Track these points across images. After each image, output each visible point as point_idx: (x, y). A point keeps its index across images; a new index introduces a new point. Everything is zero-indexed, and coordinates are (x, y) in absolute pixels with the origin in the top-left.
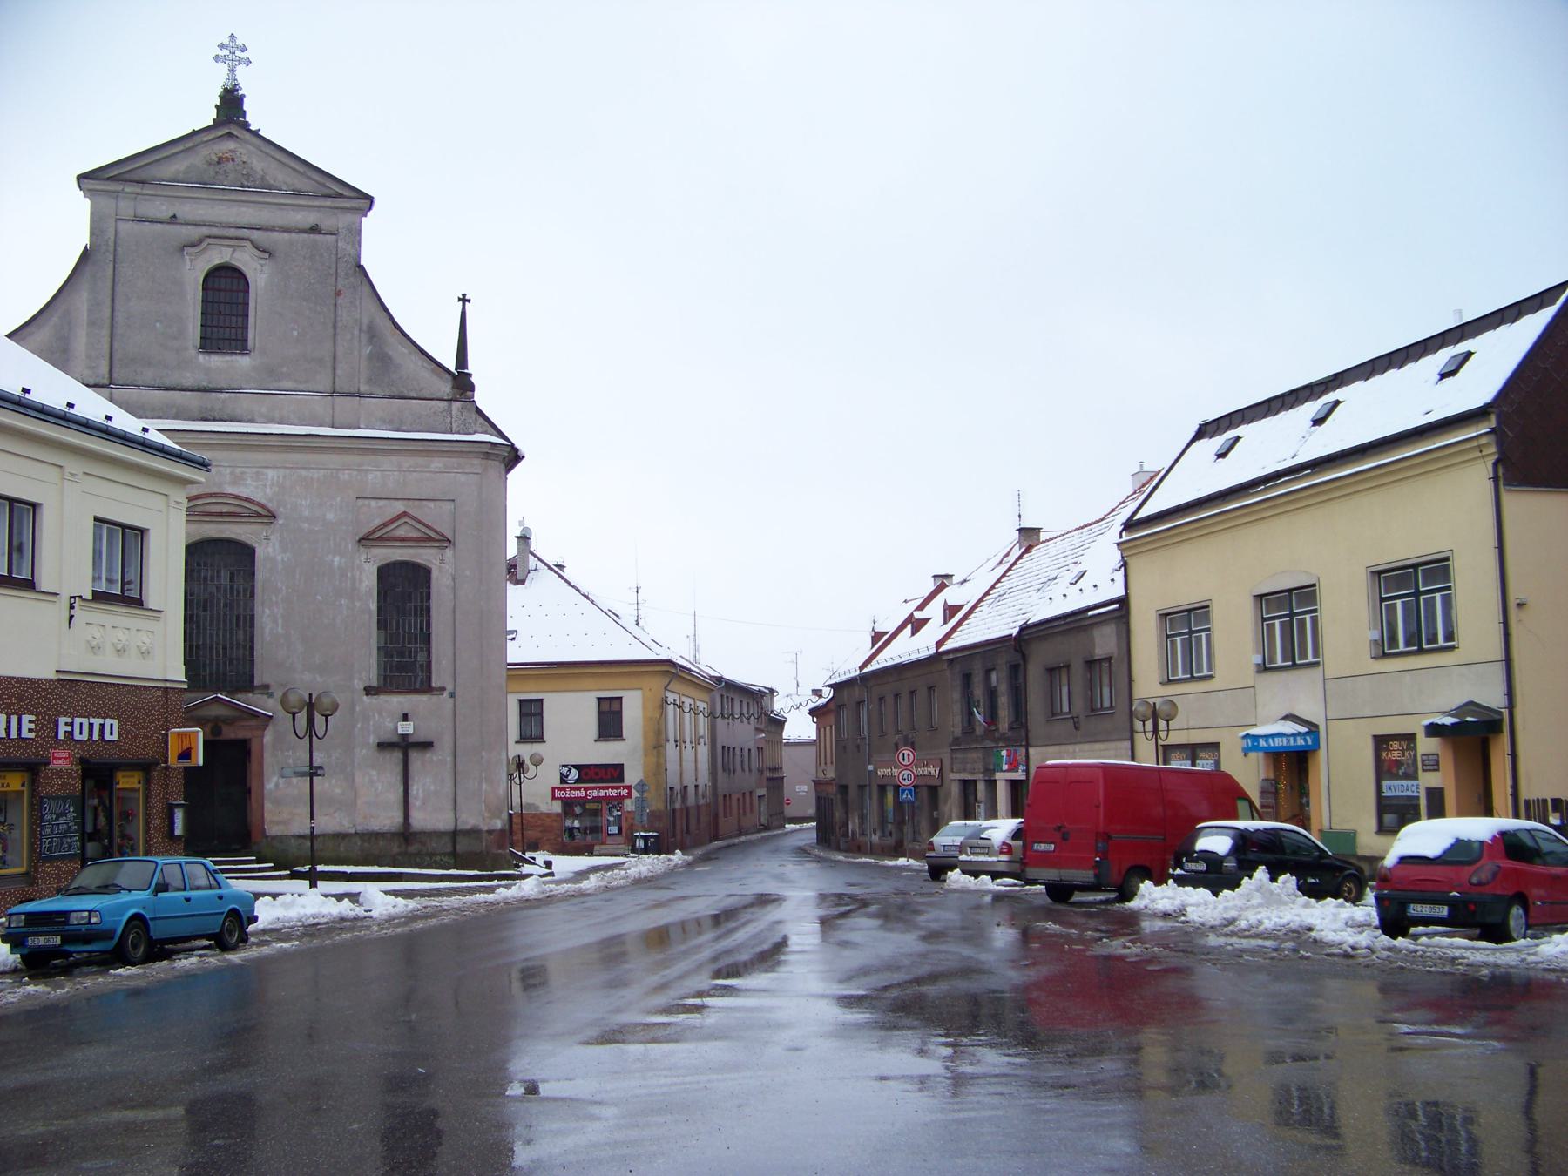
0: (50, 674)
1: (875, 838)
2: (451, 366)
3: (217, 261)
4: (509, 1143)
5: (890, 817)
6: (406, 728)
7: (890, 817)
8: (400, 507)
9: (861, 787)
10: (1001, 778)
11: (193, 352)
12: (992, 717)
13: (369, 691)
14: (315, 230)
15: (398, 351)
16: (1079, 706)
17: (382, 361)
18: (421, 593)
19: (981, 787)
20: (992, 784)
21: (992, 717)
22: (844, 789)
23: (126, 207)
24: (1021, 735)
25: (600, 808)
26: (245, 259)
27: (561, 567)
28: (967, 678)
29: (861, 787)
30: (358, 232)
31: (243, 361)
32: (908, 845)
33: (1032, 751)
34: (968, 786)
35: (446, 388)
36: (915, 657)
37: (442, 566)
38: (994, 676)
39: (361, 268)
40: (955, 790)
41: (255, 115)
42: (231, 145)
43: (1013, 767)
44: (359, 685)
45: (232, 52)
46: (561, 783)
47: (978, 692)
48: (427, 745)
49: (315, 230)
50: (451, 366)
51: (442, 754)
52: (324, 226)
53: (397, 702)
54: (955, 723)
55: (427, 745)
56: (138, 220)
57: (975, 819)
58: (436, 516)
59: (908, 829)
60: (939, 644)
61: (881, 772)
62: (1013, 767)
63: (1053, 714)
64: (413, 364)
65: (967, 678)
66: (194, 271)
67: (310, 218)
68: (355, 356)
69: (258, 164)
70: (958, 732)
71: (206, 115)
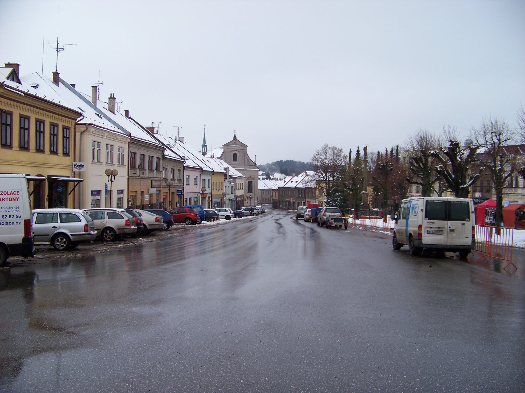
0: (241, 195)
1: (285, 208)
2: (254, 162)
3: (237, 153)
4: (357, 184)
5: (287, 205)
6: (250, 196)
7: (287, 205)
8: (250, 176)
9: (283, 201)
10: (303, 202)
11: (232, 161)
12: (302, 195)
13: (247, 193)
14: (243, 149)
15: (250, 161)
16: (311, 196)
17: (248, 162)
18: (271, 192)
19: (300, 203)
20: (301, 203)
21: (302, 195)
22: (279, 201)
23: (227, 148)
24: (305, 198)
25: (122, 197)
26: (237, 152)
27: (74, 85)
28: (299, 191)
29: (283, 201)
30: (246, 149)
31: (237, 162)
32: (290, 208)
33: (306, 200)
34: (298, 202)
35: (254, 164)
36: (292, 187)
37: (253, 181)
38: (302, 191)
39: (247, 153)
40: (297, 203)
41: (237, 138)
42: (235, 141)
43: (304, 201)
44: (246, 192)
45: (235, 131)
46: (172, 192)
47: (300, 192)
48: (252, 198)
49: (243, 149)
50: (254, 162)
51: (253, 199)
52: (244, 149)
53: (249, 194)
54: (297, 195)
55: (252, 198)
56: (228, 149)
57: (44, 208)
58: (253, 177)
59: (290, 207)
60: (296, 186)
61: (286, 200)
62: (304, 201)
63: (308, 196)
64: (251, 162)
65: (299, 191)
66: (232, 154)
67: (242, 148)
68: (246, 163)
69: (238, 143)
70: (298, 196)
71: (232, 139)
